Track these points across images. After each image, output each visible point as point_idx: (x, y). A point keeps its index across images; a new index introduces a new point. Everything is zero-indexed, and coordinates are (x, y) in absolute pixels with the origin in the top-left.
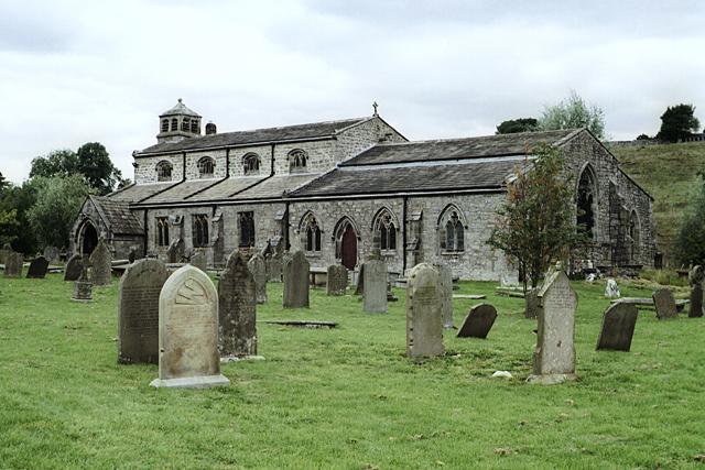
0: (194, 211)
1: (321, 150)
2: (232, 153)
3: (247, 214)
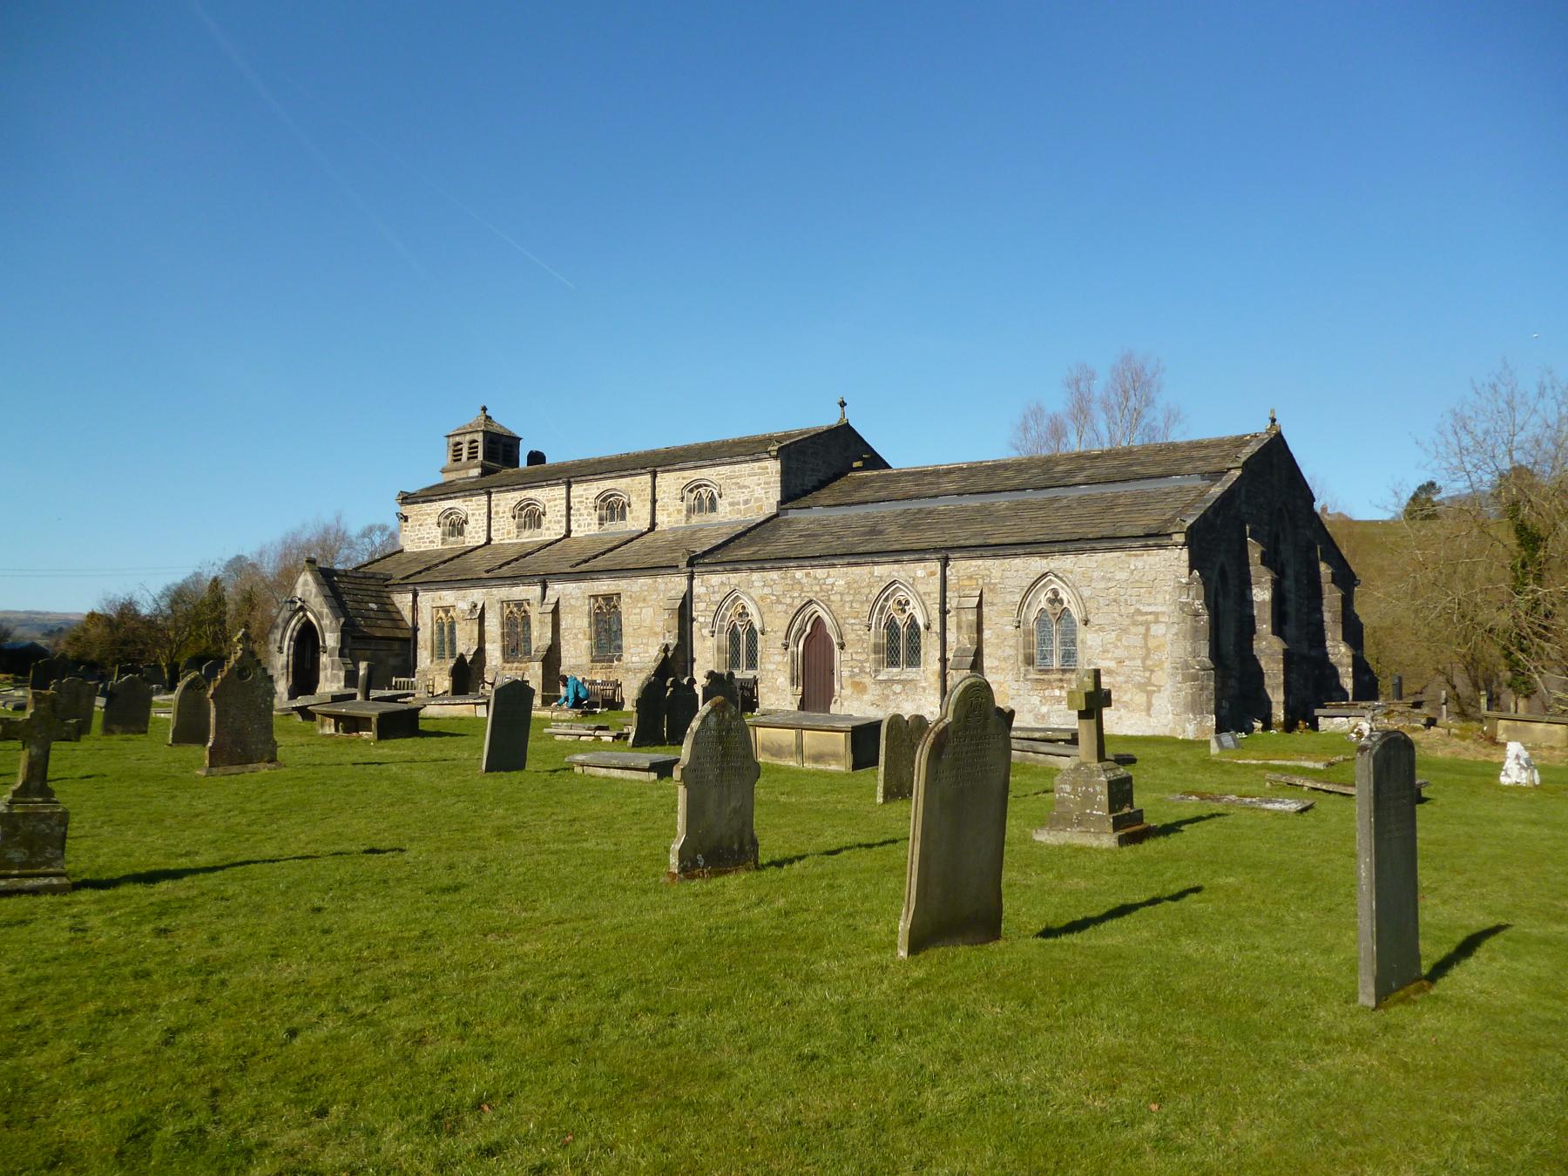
1: (748, 481)
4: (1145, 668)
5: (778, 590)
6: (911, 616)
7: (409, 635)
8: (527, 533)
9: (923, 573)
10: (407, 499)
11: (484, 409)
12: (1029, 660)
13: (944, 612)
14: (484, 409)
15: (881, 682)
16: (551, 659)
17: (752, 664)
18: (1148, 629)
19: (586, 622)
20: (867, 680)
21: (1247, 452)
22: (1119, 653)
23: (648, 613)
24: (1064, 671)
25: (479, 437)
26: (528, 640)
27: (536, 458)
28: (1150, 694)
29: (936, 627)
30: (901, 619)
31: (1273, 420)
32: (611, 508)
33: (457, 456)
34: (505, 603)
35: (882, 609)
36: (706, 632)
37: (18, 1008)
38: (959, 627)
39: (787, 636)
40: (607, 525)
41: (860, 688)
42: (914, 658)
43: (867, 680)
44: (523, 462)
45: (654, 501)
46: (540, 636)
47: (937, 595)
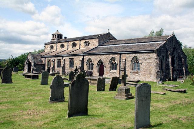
2: (69, 43)
4: (150, 71)
5: (96, 58)
6: (115, 62)
7: (44, 64)
8: (62, 49)
9: (117, 57)
10: (46, 44)
11: (57, 30)
12: (133, 69)
13: (120, 62)
14: (57, 30)
15: (111, 72)
16: (64, 68)
17: (92, 69)
18: (150, 65)
19: (69, 62)
20: (109, 72)
21: (168, 38)
22: (146, 68)
23: (77, 61)
24: (138, 71)
25: (57, 35)
26: (61, 65)
27: (65, 38)
28: (150, 75)
29: (119, 64)
30: (114, 62)
31: (173, 33)
32: (52, 47)
33: (53, 37)
34: (58, 59)
35: (111, 61)
36: (86, 64)
37: (103, 113)
38: (122, 64)
39: (97, 65)
40: (86, 47)
41: (108, 73)
42: (116, 69)
43: (109, 72)
44: (63, 38)
45: (80, 44)
46: (62, 65)
47: (119, 59)
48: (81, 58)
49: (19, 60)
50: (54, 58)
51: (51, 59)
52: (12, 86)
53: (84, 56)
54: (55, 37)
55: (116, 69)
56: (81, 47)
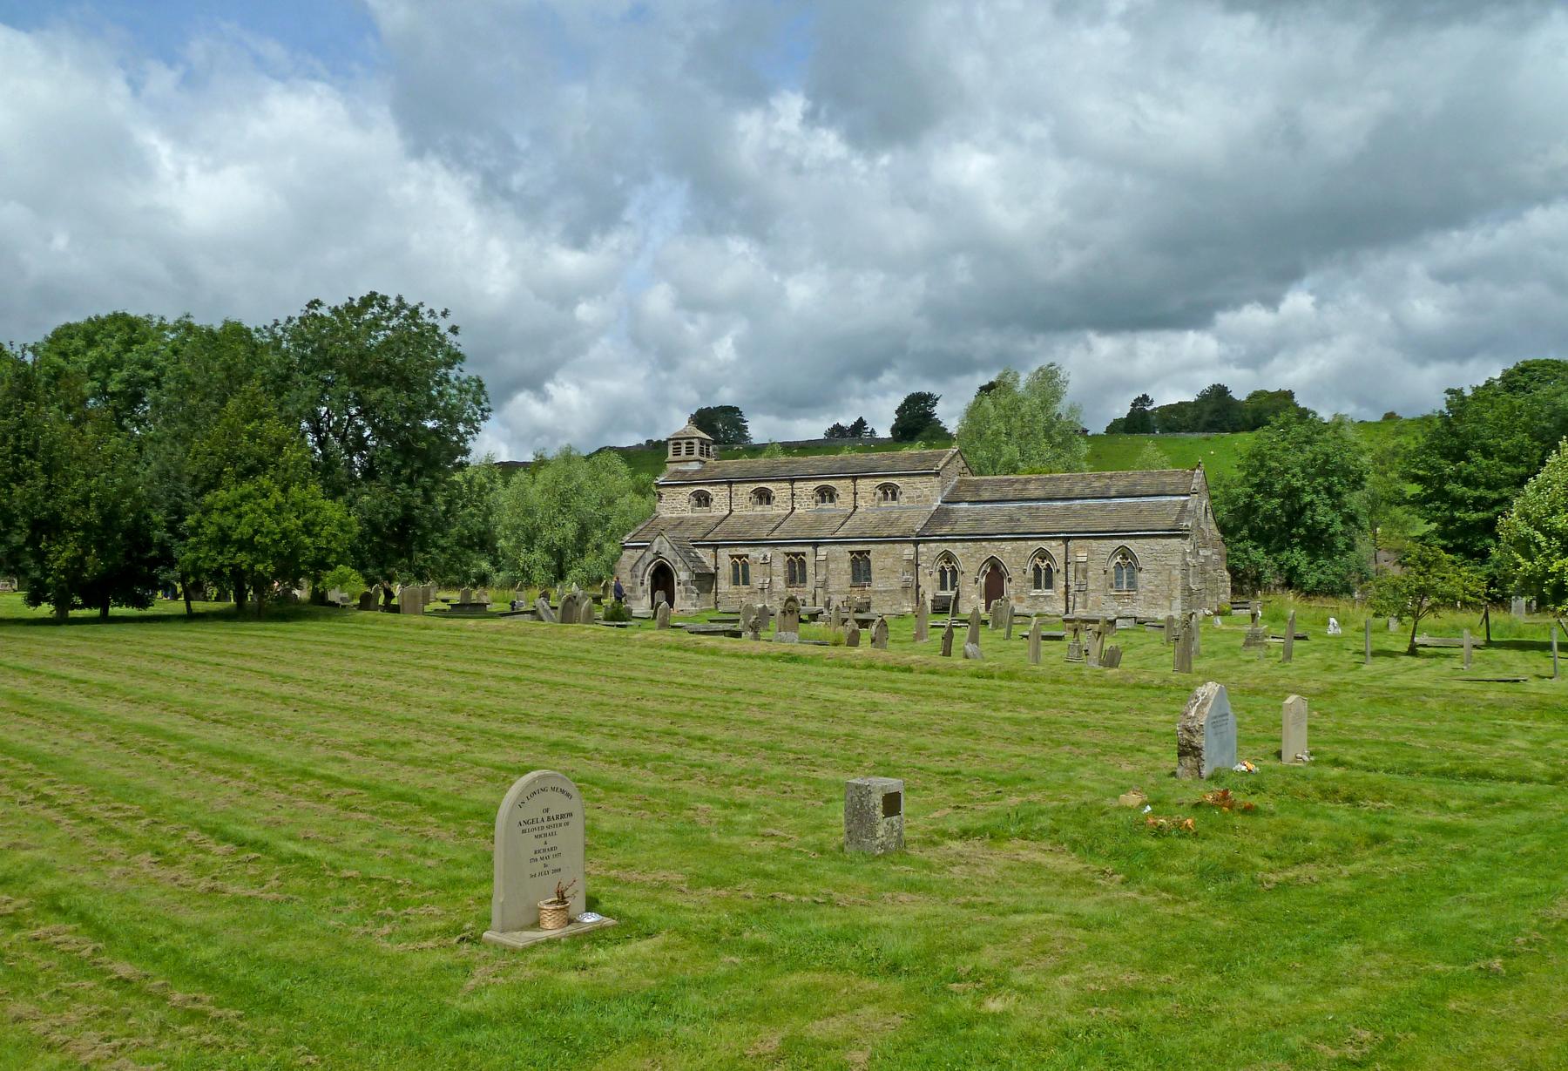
0: (787, 549)
2: (797, 485)
3: (860, 553)
8: (759, 508)
9: (1055, 548)
13: (1067, 563)
30: (1043, 565)
42: (1049, 585)
48: (908, 550)
49: (1251, 508)
50: (768, 552)
51: (755, 554)
52: (1005, 695)
53: (1246, 522)
54: (690, 452)
55: (1049, 585)
56: (860, 502)
